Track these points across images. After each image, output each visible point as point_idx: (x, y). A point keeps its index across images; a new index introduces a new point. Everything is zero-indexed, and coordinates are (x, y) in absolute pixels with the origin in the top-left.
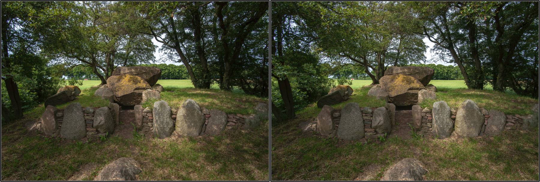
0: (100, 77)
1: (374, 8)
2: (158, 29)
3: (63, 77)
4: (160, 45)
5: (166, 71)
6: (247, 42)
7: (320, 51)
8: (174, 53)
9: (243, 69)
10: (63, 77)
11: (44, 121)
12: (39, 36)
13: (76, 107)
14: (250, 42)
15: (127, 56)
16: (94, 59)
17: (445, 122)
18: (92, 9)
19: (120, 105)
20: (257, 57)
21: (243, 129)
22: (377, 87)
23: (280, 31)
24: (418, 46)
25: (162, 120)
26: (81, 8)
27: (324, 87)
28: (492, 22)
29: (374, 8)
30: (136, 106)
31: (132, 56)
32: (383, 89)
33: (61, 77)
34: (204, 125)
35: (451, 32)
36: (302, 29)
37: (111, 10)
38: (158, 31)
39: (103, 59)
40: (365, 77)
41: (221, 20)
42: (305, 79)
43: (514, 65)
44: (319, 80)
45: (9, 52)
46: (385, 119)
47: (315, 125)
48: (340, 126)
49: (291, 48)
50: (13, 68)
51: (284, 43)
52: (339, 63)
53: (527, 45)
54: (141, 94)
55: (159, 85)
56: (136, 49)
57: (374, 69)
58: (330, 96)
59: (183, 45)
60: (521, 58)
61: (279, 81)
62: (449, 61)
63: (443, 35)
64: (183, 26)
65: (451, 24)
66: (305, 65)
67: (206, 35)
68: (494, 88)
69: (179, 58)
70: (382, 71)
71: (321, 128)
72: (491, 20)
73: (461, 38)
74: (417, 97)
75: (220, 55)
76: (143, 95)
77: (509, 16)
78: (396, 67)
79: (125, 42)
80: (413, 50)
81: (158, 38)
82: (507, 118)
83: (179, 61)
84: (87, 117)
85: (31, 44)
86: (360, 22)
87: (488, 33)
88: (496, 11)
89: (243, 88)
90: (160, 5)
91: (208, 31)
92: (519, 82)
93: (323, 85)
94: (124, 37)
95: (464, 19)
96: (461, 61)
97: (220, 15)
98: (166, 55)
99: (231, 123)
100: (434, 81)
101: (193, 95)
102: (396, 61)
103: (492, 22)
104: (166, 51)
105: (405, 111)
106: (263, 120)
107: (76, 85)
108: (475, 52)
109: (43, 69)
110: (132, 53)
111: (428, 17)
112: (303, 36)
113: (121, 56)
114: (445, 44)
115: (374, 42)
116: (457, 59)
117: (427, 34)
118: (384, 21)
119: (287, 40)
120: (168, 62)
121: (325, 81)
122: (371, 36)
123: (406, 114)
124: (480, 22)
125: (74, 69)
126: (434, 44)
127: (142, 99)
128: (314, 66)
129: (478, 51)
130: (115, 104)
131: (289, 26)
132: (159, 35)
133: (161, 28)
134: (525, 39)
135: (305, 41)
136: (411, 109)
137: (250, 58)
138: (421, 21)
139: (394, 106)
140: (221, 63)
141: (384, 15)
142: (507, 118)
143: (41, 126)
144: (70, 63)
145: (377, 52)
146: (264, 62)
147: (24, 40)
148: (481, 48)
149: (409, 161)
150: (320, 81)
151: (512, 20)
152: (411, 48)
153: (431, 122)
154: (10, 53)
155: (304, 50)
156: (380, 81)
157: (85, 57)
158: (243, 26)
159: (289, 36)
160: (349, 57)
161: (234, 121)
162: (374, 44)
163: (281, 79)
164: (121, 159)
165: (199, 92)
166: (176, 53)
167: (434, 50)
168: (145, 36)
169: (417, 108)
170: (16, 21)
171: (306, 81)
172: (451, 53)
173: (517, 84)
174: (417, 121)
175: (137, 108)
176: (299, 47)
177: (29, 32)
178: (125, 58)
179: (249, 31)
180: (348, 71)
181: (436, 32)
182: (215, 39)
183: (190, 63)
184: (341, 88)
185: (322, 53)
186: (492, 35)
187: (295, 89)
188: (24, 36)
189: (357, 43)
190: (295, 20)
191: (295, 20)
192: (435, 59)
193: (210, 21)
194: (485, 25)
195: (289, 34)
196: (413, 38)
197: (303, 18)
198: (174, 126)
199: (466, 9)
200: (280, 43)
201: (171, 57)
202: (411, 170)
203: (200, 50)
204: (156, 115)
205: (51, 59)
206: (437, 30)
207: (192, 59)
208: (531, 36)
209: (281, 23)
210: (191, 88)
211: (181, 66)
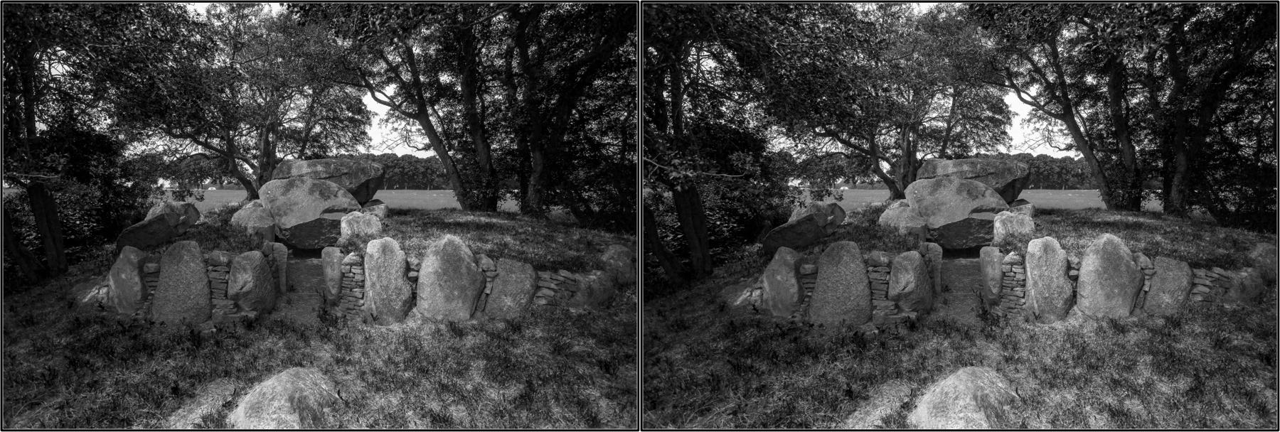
0: (244, 182)
1: (891, 25)
2: (379, 73)
3: (161, 181)
4: (383, 110)
5: (397, 170)
6: (584, 106)
7: (770, 124)
8: (414, 129)
9: (575, 168)
10: (161, 181)
11: (116, 282)
12: (106, 89)
13: (189, 251)
14: (592, 104)
15: (307, 135)
16: (230, 142)
17: (1054, 286)
18: (227, 28)
19: (289, 246)
20: (606, 140)
21: (1227, 301)
22: (901, 205)
23: (676, 80)
24: (994, 112)
25: (385, 283)
26: (204, 25)
27: (778, 206)
28: (1161, 58)
29: (891, 25)
30: (327, 250)
31: (318, 135)
32: (913, 210)
33: (156, 182)
34: (484, 296)
35: (1068, 81)
36: (727, 74)
37: (270, 29)
38: (378, 79)
39: (252, 143)
40: (872, 183)
41: (523, 54)
42: (736, 189)
43: (1211, 157)
44: (767, 189)
45: (37, 124)
46: (918, 279)
47: (758, 292)
48: (815, 296)
49: (703, 117)
50: (46, 162)
51: (687, 105)
52: (814, 150)
53: (1240, 111)
54: (339, 222)
55: (378, 202)
56: (327, 118)
57: (893, 165)
58: (792, 226)
59: (435, 111)
60: (1225, 141)
61: (675, 192)
62: (1063, 146)
63: (1049, 87)
64: (434, 67)
65: (1069, 63)
66: (734, 156)
67: (488, 88)
68: (1165, 208)
69: (427, 141)
70: (910, 169)
71: (118, 297)
72: (1159, 53)
73: (1089, 93)
74: (992, 227)
75: (521, 133)
76: (343, 225)
77: (1198, 43)
78: (945, 161)
79: (303, 102)
80: (982, 121)
81: (378, 95)
82: (538, 278)
83: (427, 148)
84: (213, 275)
85: (88, 105)
86: (861, 58)
87: (1153, 84)
88: (1169, 34)
89: (575, 211)
90: (382, 19)
91: (494, 79)
92: (1222, 195)
93: (776, 201)
94: (301, 92)
95: (1097, 51)
96: (1092, 147)
97: (521, 40)
98: (395, 134)
99: (545, 291)
100: (1029, 192)
101: (458, 225)
102: (944, 147)
103: (1161, 58)
104: (396, 125)
105: (963, 261)
106: (623, 285)
107: (189, 200)
108: (1123, 125)
109: (113, 164)
110: (318, 129)
111: (1012, 46)
112: (729, 89)
113: (293, 135)
114: (1053, 108)
115: (893, 104)
116: (1082, 141)
117: (1013, 86)
118: (916, 55)
119: (693, 98)
120: (401, 151)
121: (782, 192)
122: (885, 90)
123: (965, 266)
124: (1135, 58)
125: (184, 163)
126: (1030, 108)
127: (339, 233)
128: (757, 157)
129: (1130, 123)
130: (277, 245)
131: (699, 67)
132: (380, 87)
133: (387, 71)
134: (1234, 96)
135: (736, 101)
136: (978, 256)
137: (590, 141)
138: (1001, 57)
139: (940, 249)
140: (523, 153)
141: (916, 41)
142: (538, 278)
143: (108, 293)
144: (177, 151)
145: (899, 126)
146: (622, 152)
147: (71, 98)
148: (1135, 116)
149: (973, 373)
150: (769, 193)
151: (1205, 54)
152: (978, 118)
153: (1024, 286)
154: (41, 126)
155: (732, 121)
156: (907, 191)
157: (211, 136)
158: (575, 67)
159: (697, 89)
160: (834, 135)
161: (553, 286)
162: (892, 105)
163: (679, 188)
164: (292, 370)
165: (470, 218)
166: (419, 130)
167: (1029, 121)
168: (349, 90)
169: (991, 254)
170: (55, 53)
171: (737, 193)
172: (1069, 127)
173: (1218, 199)
174: (991, 283)
175: (328, 254)
176: (721, 115)
177: (83, 80)
178: (300, 139)
179: (588, 79)
180: (833, 169)
181: (1033, 81)
182: (511, 99)
183: (450, 153)
184: (818, 209)
185: (775, 128)
186: (1160, 88)
187: (711, 209)
188: (71, 89)
189: (855, 106)
190: (712, 53)
191: (712, 53)
192: (1031, 143)
193: (499, 56)
194: (1144, 65)
195: (697, 84)
196: (982, 94)
197: (730, 47)
198: (414, 296)
199: (1103, 30)
200: (677, 104)
201: (407, 139)
202: (979, 394)
203: (475, 122)
204: (371, 270)
205: (132, 140)
206: (1037, 76)
207: (455, 142)
208: (1249, 90)
209: (679, 60)
210: (453, 210)
211: (429, 160)
